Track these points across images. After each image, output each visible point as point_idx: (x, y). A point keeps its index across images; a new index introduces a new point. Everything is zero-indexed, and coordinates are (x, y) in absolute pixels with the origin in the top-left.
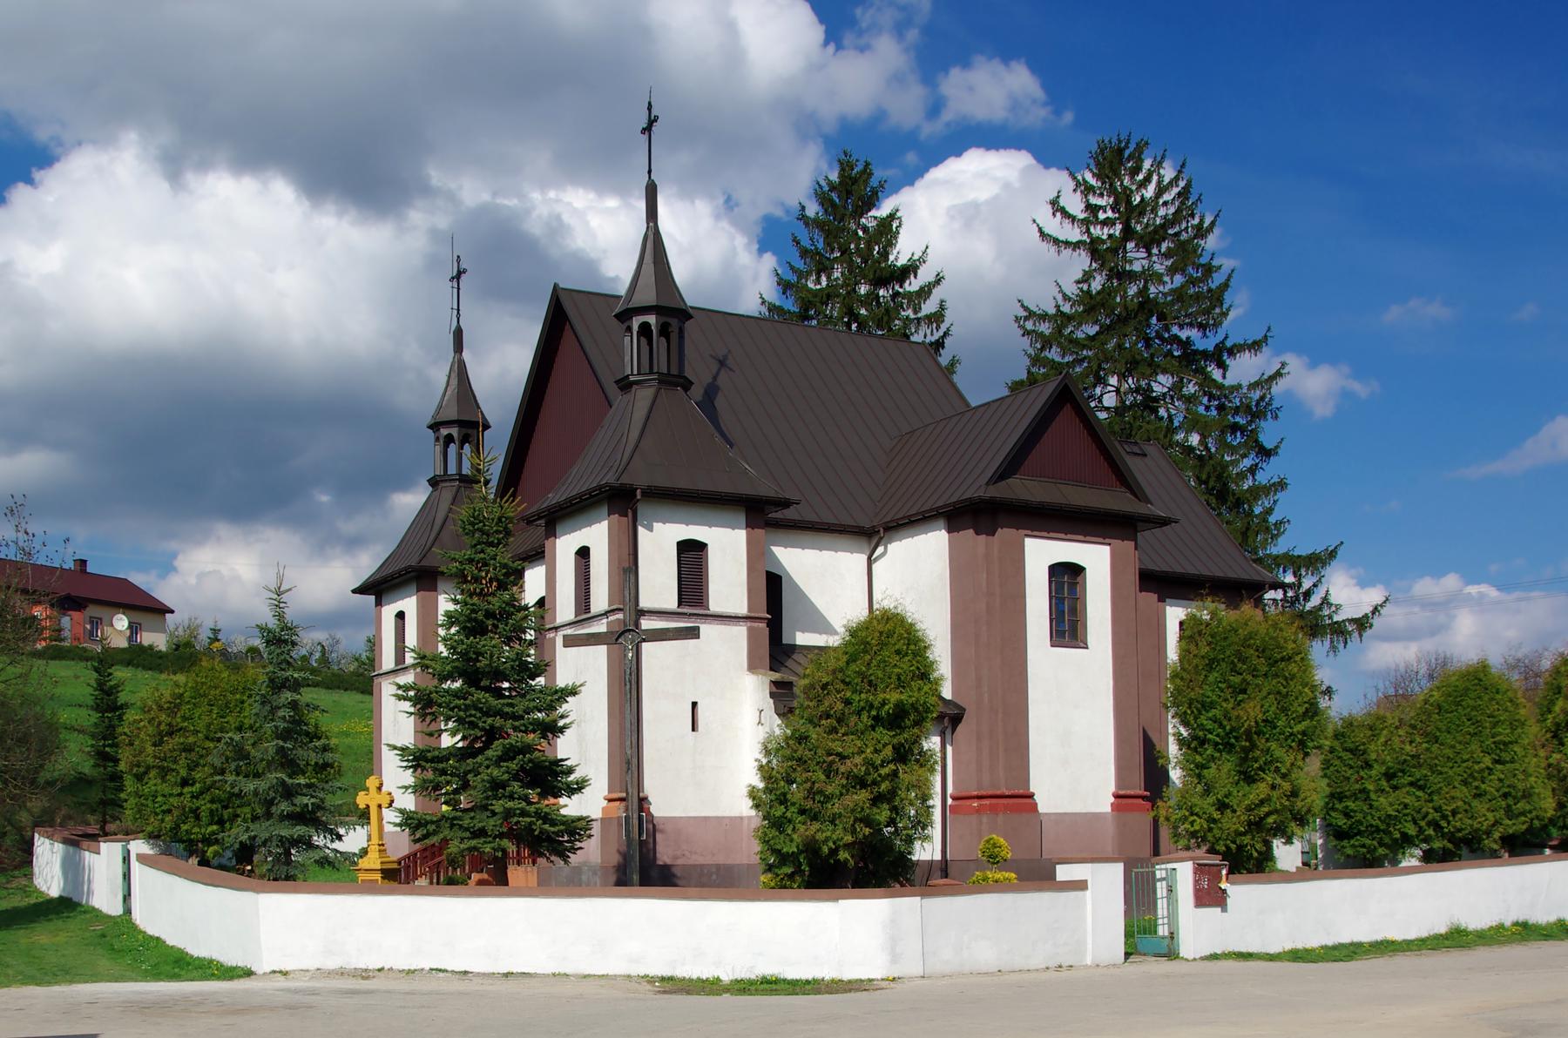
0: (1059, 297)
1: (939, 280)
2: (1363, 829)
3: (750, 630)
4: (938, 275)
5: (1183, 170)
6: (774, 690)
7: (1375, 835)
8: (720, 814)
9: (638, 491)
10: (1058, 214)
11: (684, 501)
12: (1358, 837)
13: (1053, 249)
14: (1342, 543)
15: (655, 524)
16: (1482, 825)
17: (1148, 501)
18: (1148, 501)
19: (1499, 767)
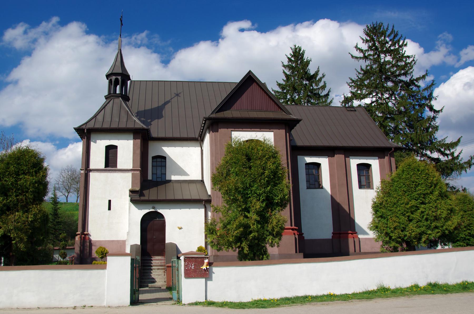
0: (357, 73)
1: (324, 76)
2: (459, 239)
3: (132, 174)
4: (323, 74)
5: (394, 28)
6: (131, 194)
7: (464, 241)
8: (119, 239)
9: (86, 129)
10: (358, 50)
11: (104, 132)
12: (458, 242)
13: (356, 60)
14: (462, 137)
15: (97, 141)
16: (411, 234)
17: (291, 114)
18: (291, 114)
19: (423, 206)
